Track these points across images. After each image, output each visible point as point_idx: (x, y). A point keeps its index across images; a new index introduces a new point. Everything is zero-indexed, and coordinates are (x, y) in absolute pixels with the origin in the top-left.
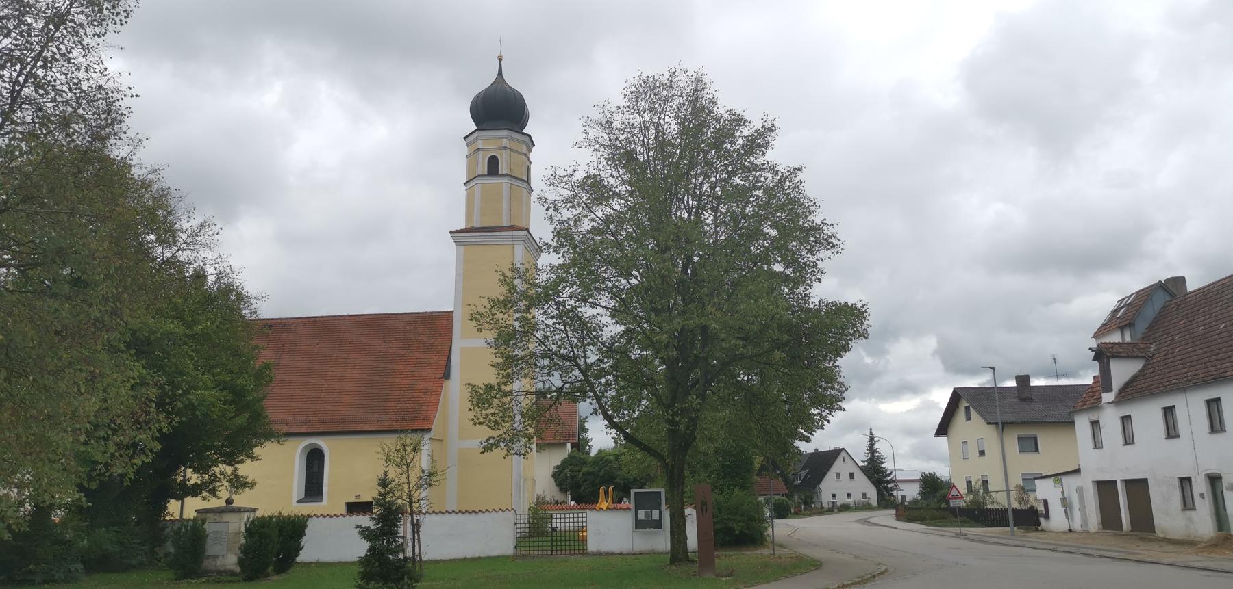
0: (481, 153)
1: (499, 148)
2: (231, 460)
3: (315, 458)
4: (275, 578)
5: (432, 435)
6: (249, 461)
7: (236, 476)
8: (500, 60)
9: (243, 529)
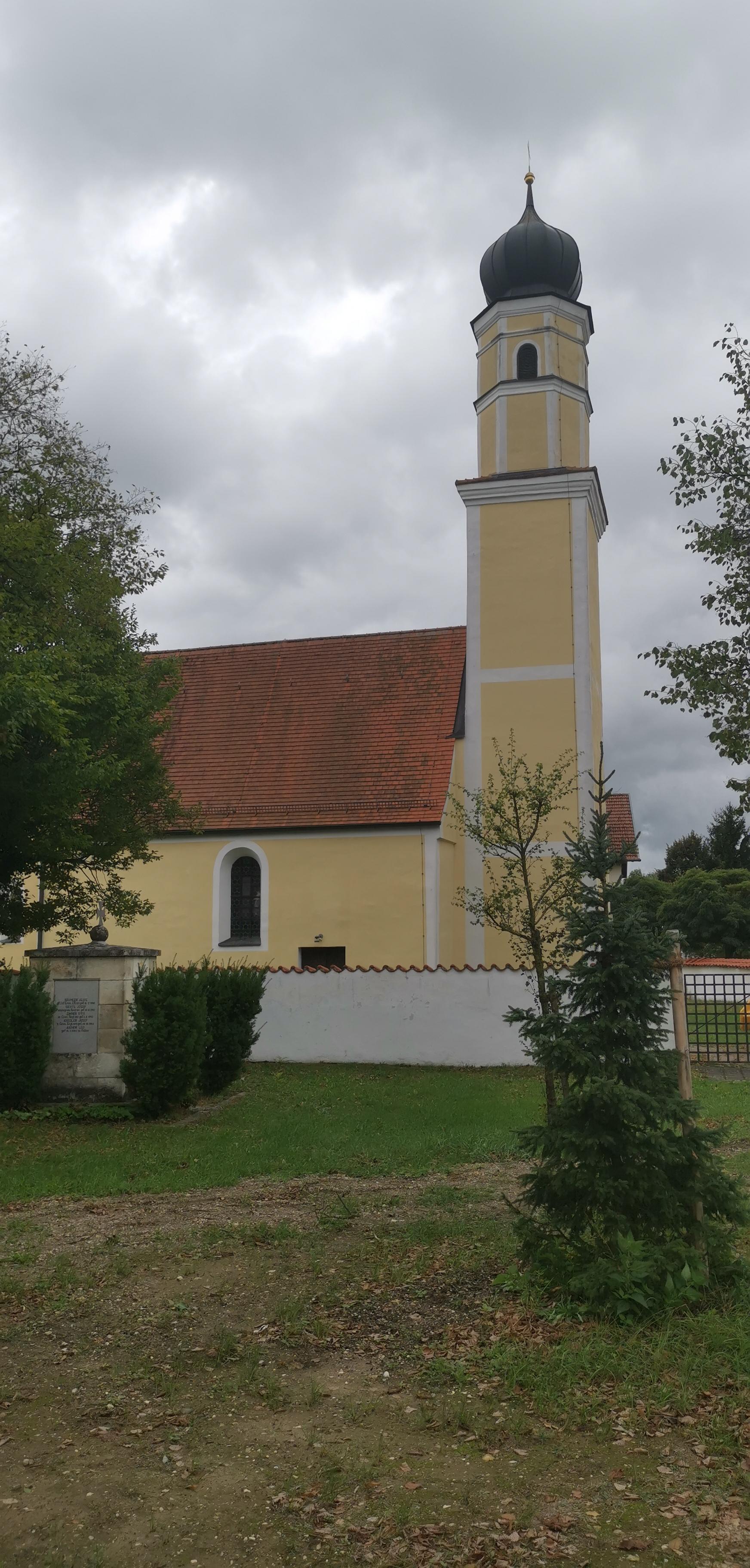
0: (504, 342)
1: (537, 331)
2: (104, 858)
3: (245, 874)
4: (202, 1107)
5: (442, 832)
6: (138, 863)
7: (117, 892)
8: (529, 182)
9: (130, 997)
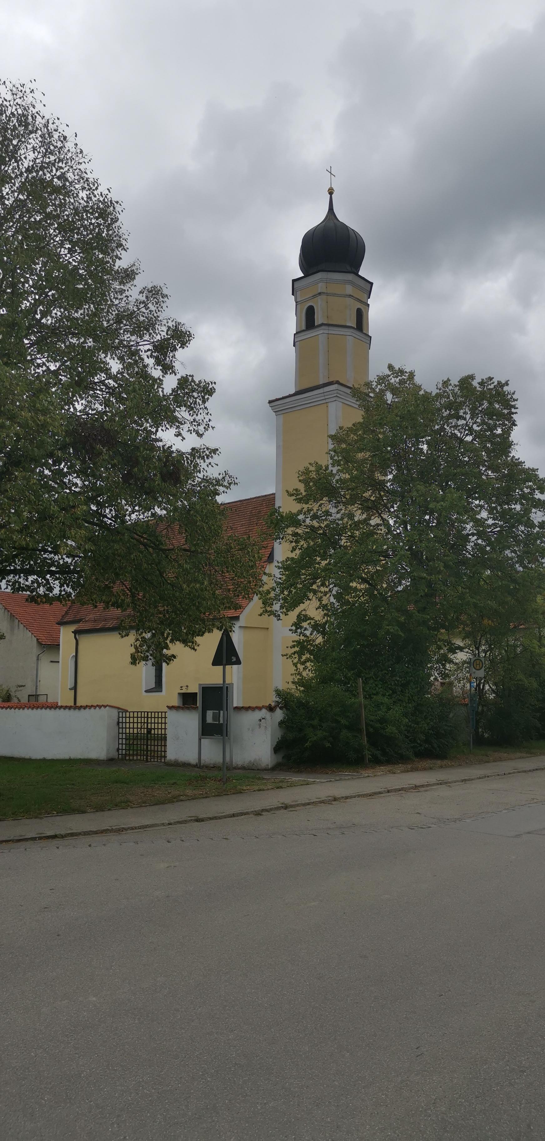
1: (314, 296)
